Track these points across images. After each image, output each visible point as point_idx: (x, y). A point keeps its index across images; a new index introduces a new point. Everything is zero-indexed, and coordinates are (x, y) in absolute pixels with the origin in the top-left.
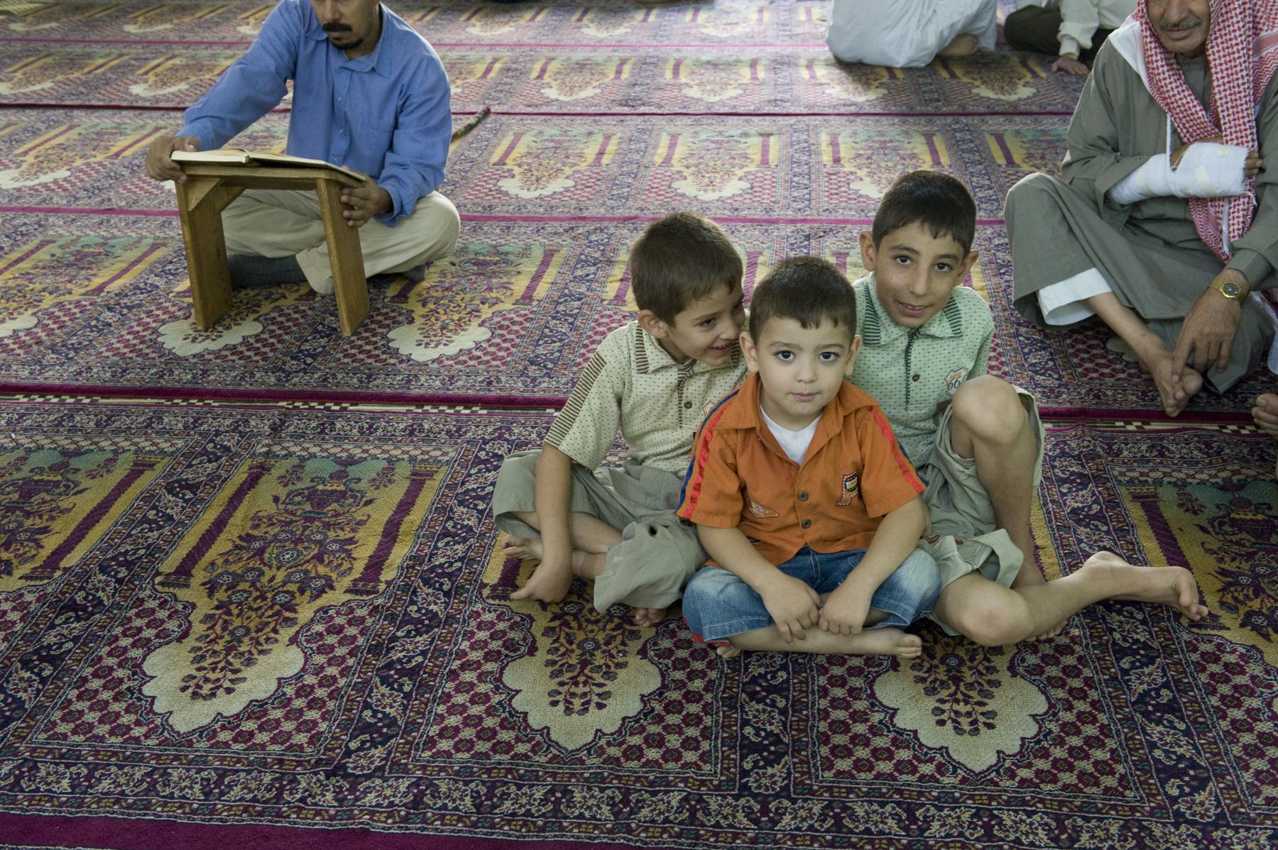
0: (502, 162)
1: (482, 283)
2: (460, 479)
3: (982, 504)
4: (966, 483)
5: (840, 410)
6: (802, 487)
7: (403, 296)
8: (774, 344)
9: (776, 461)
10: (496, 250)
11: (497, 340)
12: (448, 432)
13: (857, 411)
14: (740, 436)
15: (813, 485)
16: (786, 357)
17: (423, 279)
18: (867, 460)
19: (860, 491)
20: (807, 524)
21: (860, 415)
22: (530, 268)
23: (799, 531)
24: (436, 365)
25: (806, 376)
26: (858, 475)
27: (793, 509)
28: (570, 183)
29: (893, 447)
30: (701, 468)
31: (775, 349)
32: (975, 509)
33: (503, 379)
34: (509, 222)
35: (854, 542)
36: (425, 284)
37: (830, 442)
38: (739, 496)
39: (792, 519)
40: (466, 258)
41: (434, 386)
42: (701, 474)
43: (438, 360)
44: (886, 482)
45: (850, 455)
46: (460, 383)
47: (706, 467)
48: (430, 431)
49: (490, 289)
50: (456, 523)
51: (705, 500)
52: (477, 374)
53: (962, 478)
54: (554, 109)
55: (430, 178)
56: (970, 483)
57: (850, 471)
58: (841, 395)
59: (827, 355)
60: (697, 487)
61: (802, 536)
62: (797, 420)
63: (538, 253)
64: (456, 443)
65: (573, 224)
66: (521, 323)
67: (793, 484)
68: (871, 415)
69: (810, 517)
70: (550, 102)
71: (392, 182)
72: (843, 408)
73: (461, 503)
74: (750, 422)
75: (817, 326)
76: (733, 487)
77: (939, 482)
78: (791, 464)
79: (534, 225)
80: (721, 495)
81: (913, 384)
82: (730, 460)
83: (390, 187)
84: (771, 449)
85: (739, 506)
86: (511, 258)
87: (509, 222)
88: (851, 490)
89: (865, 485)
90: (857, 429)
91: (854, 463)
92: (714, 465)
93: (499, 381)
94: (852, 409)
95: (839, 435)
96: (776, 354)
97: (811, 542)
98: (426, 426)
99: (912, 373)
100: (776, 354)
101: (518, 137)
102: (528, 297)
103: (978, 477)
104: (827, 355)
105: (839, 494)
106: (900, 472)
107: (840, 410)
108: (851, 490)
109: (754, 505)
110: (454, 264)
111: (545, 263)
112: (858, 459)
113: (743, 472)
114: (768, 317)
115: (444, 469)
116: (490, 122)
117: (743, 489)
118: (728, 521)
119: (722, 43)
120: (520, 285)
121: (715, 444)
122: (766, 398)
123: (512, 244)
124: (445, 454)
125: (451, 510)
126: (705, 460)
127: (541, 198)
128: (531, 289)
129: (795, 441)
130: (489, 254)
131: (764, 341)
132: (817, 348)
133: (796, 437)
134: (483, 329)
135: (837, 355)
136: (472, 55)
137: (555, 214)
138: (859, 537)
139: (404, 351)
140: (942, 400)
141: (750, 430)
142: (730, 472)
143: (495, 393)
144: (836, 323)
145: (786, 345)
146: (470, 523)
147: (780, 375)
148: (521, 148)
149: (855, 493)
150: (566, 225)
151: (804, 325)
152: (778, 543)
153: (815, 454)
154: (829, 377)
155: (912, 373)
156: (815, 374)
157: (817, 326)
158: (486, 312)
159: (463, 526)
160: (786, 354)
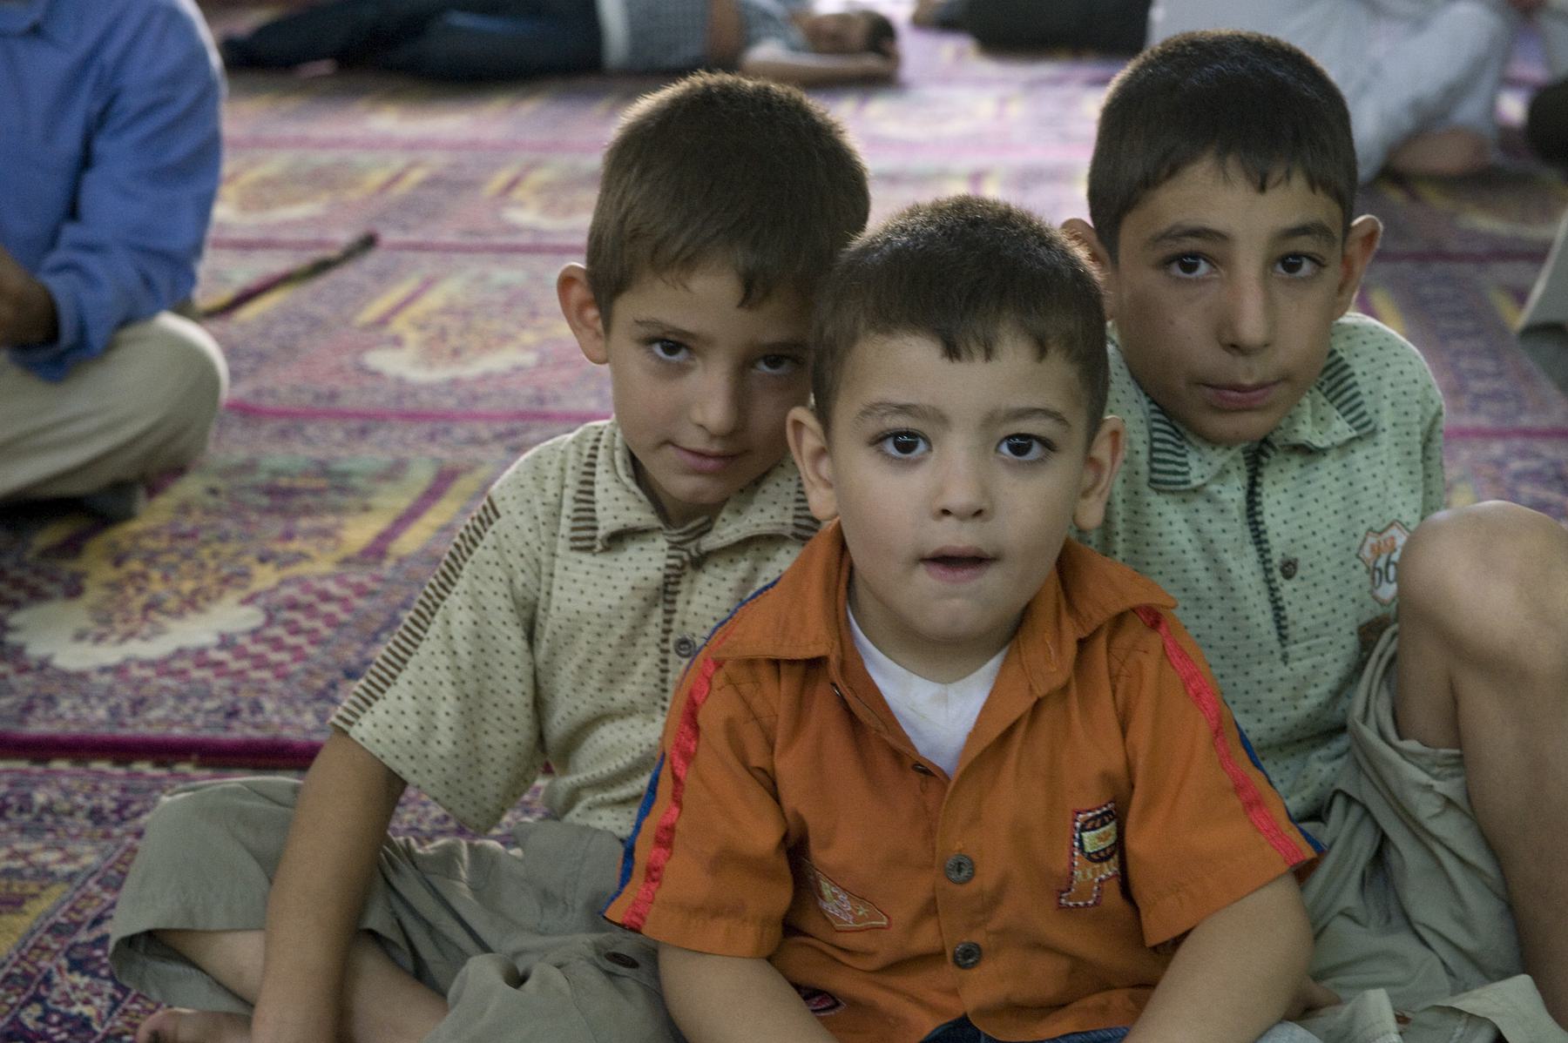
0: (383, 321)
1: (276, 525)
2: (91, 913)
3: (1483, 907)
4: (1436, 827)
5: (1068, 624)
6: (956, 843)
7: (72, 547)
8: (870, 410)
9: (885, 764)
10: (323, 470)
11: (277, 631)
12: (96, 815)
13: (1119, 620)
14: (788, 685)
15: (990, 837)
16: (906, 448)
17: (128, 516)
18: (1141, 763)
19: (1123, 865)
20: (969, 956)
21: (1124, 640)
22: (394, 500)
23: (948, 974)
24: (107, 679)
25: (960, 496)
26: (1116, 814)
27: (930, 909)
28: (530, 359)
29: (1217, 732)
30: (677, 780)
31: (873, 426)
32: (1464, 922)
33: (269, 705)
34: (365, 423)
35: (1103, 1009)
36: (135, 526)
37: (1038, 706)
38: (783, 864)
39: (926, 939)
40: (248, 480)
41: (95, 718)
42: (677, 800)
43: (119, 670)
44: (1195, 828)
45: (1093, 752)
46: (156, 714)
47: (689, 777)
48: (48, 808)
49: (288, 536)
50: (47, 1012)
51: (686, 875)
52: (207, 694)
53: (1426, 808)
54: (524, 239)
55: (161, 277)
56: (1450, 828)
57: (1092, 800)
58: (1068, 566)
59: (1020, 444)
60: (665, 840)
61: (954, 992)
62: (943, 651)
63: (421, 475)
64: (107, 836)
65: (518, 424)
66: (343, 601)
67: (930, 832)
68: (1154, 640)
69: (978, 937)
70: (514, 229)
71: (71, 277)
72: (1074, 614)
73: (77, 966)
74: (812, 641)
75: (989, 353)
76: (763, 836)
77: (1364, 845)
78: (925, 771)
79: (426, 427)
80: (727, 860)
81: (1286, 588)
82: (757, 758)
83: (60, 286)
84: (870, 730)
85: (780, 897)
86: (356, 481)
87: (365, 423)
88: (1099, 858)
89: (1137, 844)
90: (1114, 678)
91: (1106, 778)
92: (714, 763)
93: (257, 708)
94: (1099, 617)
95: (1065, 689)
96: (877, 440)
97: (983, 1012)
98: (40, 798)
99: (1276, 558)
100: (877, 440)
101: (428, 284)
102: (376, 551)
103: (1469, 807)
104: (1020, 444)
105: (1061, 866)
106: (1237, 803)
107: (1068, 624)
108: (1099, 858)
109: (827, 889)
110: (213, 492)
111: (433, 494)
112: (1116, 763)
113: (793, 797)
114: (853, 339)
115: (57, 891)
116: (372, 260)
117: (795, 848)
118: (748, 936)
119: (910, 146)
120: (359, 532)
121: (713, 714)
122: (861, 590)
123: (365, 457)
124: (72, 858)
125: (47, 981)
126: (688, 757)
127: (455, 382)
128: (386, 537)
129: (940, 711)
130: (305, 474)
131: (846, 411)
132: (991, 420)
133: (945, 700)
134: (249, 610)
135: (1048, 445)
136: (362, 158)
137: (482, 407)
138: (1118, 998)
139: (36, 649)
140: (1366, 617)
141: (815, 665)
142: (756, 793)
143: (241, 731)
144: (1042, 350)
145: (903, 409)
146: (88, 1011)
147: (895, 503)
148: (434, 300)
149: (1109, 869)
150: (501, 427)
151: (952, 351)
152: (884, 999)
153: (993, 746)
154: (1027, 504)
155: (1276, 558)
156: (985, 492)
157: (989, 353)
158: (265, 577)
159: (66, 1018)
160: (906, 442)
